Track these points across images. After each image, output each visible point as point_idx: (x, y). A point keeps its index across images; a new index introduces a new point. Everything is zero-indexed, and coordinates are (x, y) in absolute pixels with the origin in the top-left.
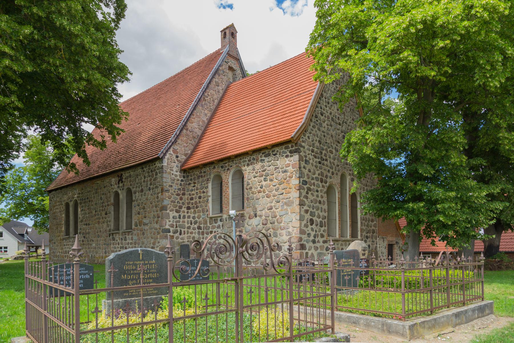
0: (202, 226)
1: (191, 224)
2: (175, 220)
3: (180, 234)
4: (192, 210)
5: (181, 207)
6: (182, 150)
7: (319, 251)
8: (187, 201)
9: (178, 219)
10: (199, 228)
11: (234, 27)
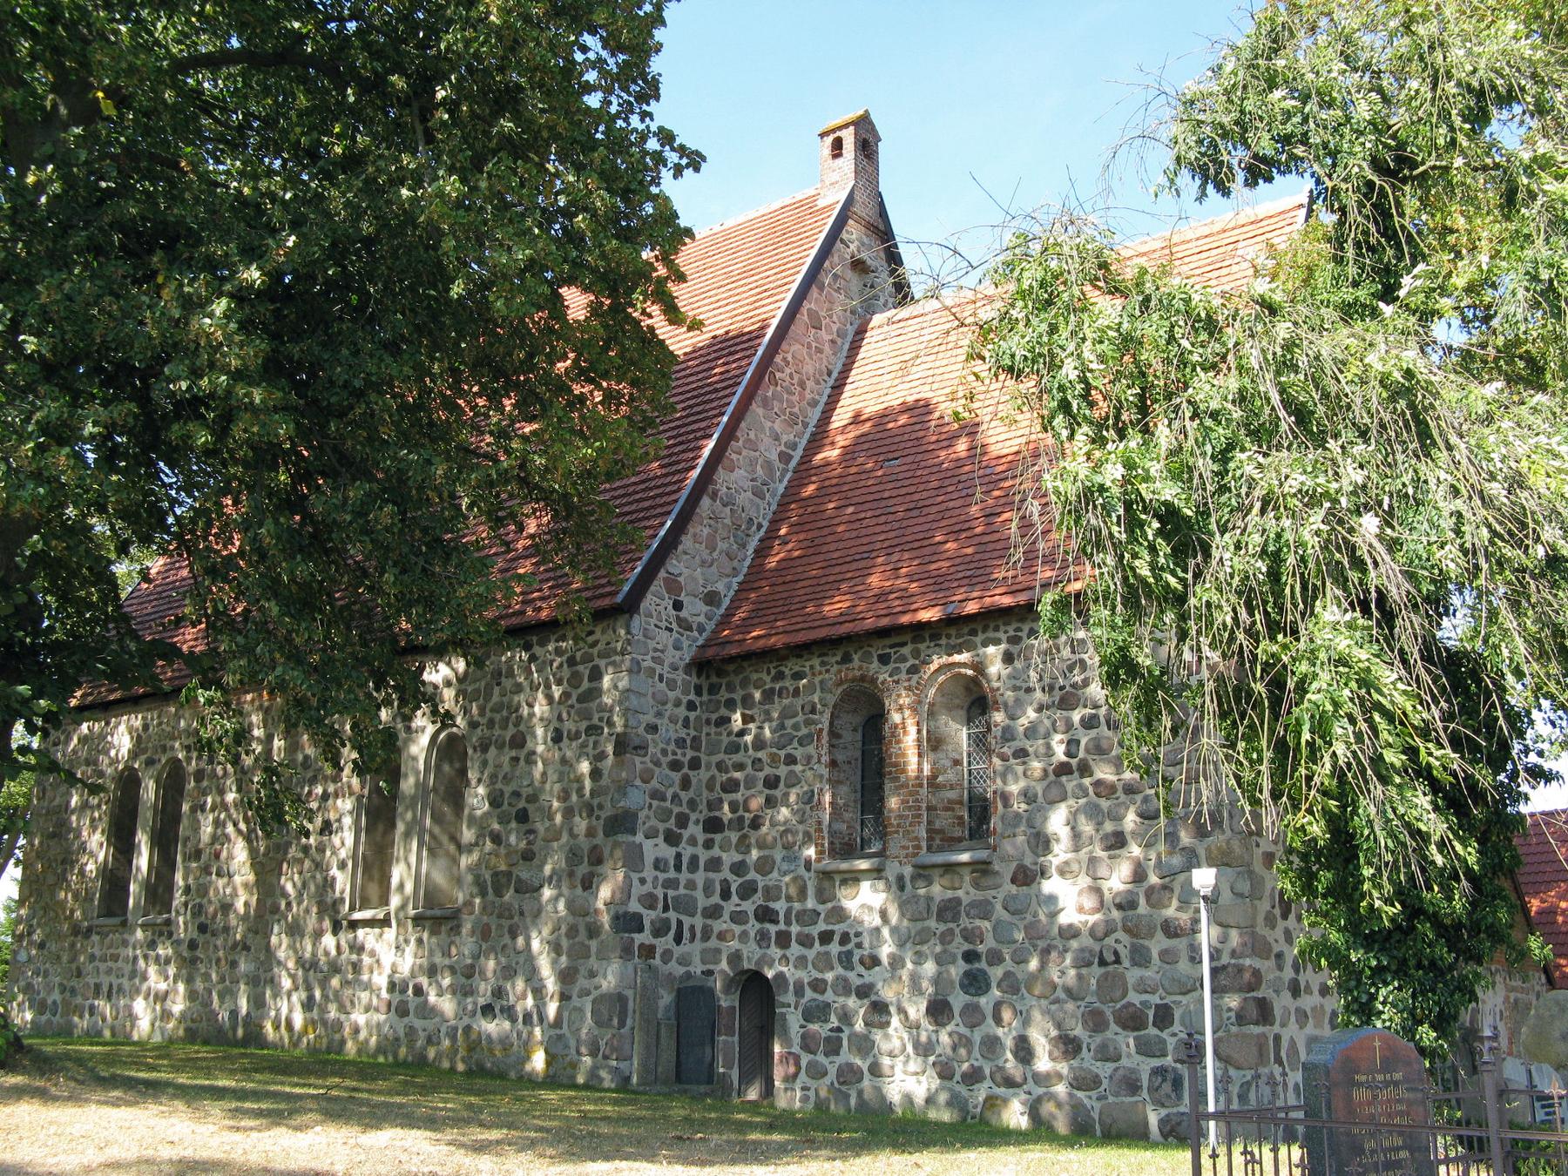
0: (780, 906)
1: (726, 895)
2: (662, 876)
3: (678, 939)
4: (734, 837)
5: (683, 821)
6: (694, 579)
7: (1310, 1029)
8: (705, 793)
9: (672, 874)
10: (766, 915)
11: (871, 123)
